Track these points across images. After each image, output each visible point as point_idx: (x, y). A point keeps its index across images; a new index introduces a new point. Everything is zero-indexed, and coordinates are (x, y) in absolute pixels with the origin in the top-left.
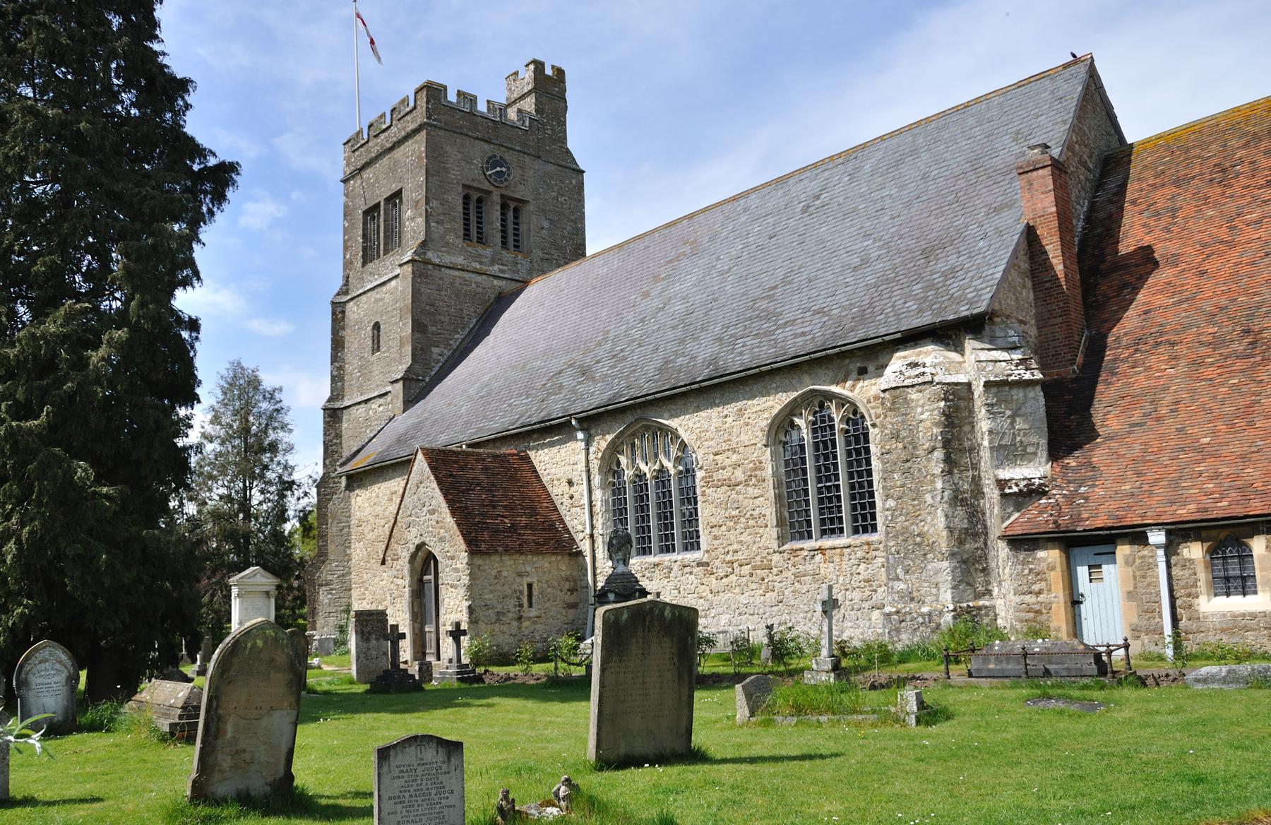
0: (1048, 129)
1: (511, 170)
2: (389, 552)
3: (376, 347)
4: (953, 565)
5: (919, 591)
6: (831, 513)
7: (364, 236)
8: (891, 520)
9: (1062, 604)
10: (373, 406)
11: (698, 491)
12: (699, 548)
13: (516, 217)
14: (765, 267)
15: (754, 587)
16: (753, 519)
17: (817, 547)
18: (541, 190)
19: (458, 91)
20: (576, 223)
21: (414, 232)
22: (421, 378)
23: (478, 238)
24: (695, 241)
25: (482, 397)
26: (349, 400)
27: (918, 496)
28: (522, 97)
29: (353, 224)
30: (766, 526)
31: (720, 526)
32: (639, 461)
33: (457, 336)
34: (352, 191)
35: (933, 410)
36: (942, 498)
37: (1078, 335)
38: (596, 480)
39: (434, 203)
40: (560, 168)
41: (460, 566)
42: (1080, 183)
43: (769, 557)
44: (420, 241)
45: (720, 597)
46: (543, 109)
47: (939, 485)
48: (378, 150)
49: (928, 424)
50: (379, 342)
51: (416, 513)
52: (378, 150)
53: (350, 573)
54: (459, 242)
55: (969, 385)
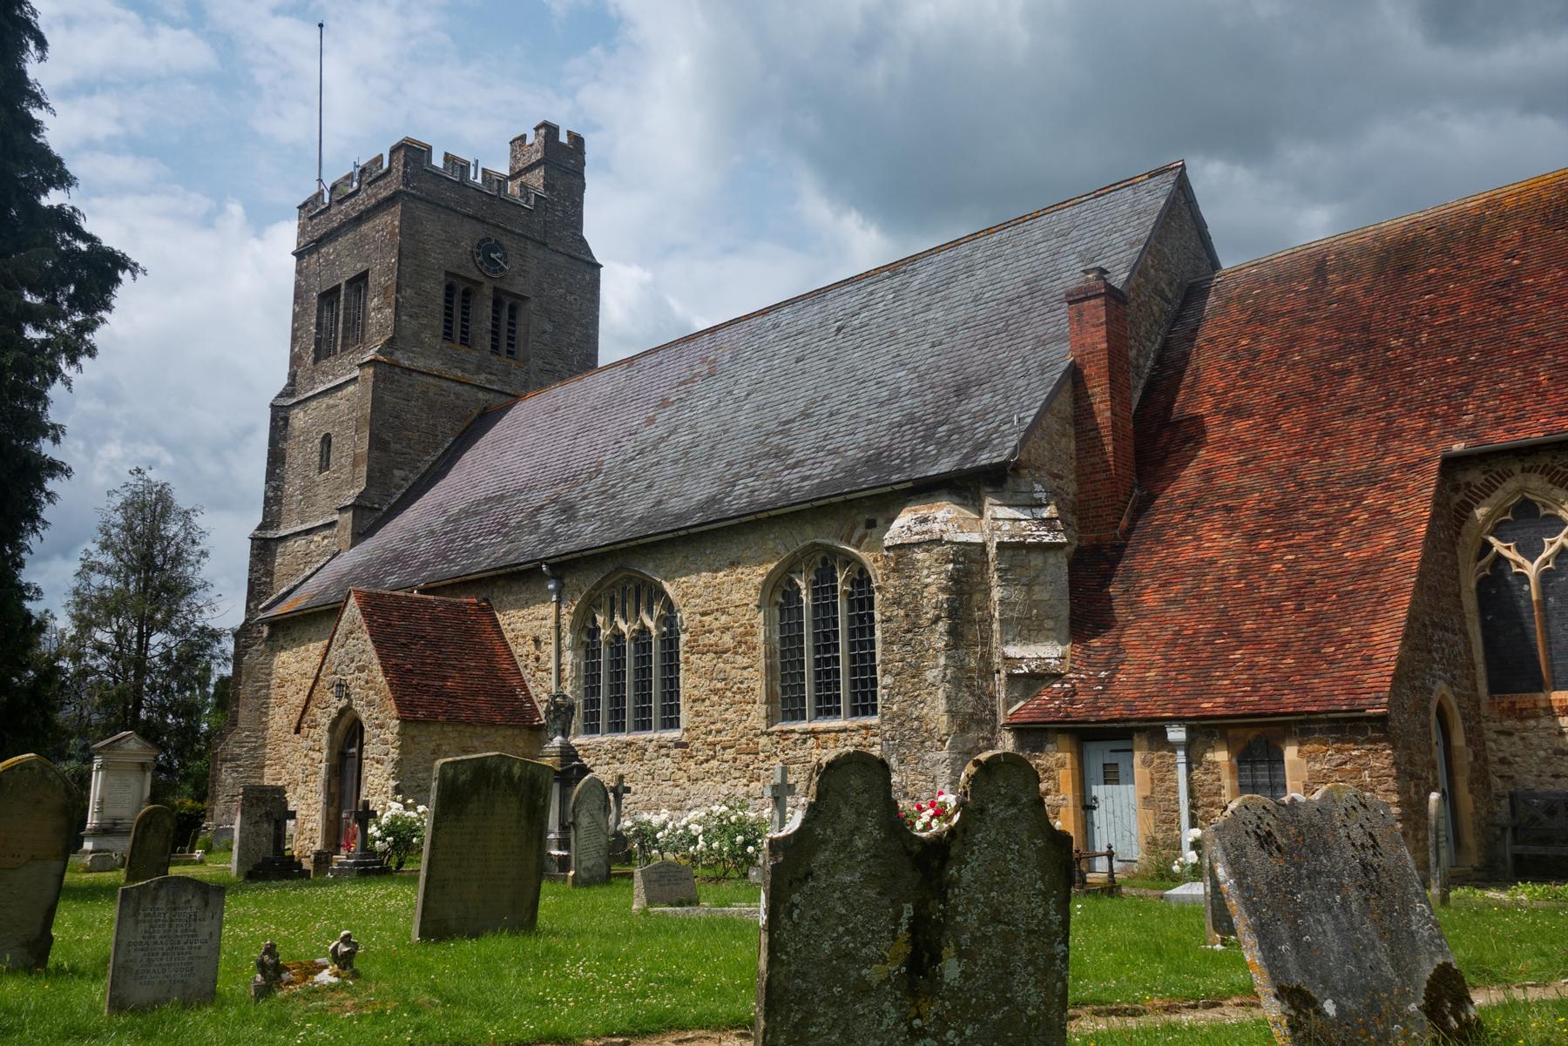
0: (1119, 250)
1: (509, 257)
2: (307, 718)
3: (324, 465)
4: (953, 756)
5: (914, 785)
6: (829, 690)
7: (319, 325)
8: (888, 700)
9: (1071, 808)
10: (316, 538)
11: (681, 658)
12: (678, 727)
13: (512, 316)
14: (786, 395)
15: (738, 775)
16: (741, 693)
17: (810, 729)
18: (545, 285)
19: (446, 154)
20: (587, 328)
21: (381, 326)
22: (376, 506)
23: (462, 338)
24: (714, 361)
25: (446, 533)
26: (286, 528)
27: (917, 671)
28: (530, 168)
29: (305, 309)
30: (755, 702)
31: (704, 700)
32: (617, 618)
33: (426, 458)
34: (307, 267)
35: (940, 573)
36: (944, 677)
37: (1125, 494)
38: (568, 639)
39: (408, 292)
40: (570, 260)
41: (389, 737)
42: (1153, 315)
43: (756, 740)
44: (387, 337)
45: (698, 786)
46: (553, 186)
47: (942, 661)
48: (341, 220)
49: (933, 589)
50: (328, 459)
51: (343, 670)
52: (341, 220)
53: (264, 746)
54: (438, 343)
55: (983, 546)
